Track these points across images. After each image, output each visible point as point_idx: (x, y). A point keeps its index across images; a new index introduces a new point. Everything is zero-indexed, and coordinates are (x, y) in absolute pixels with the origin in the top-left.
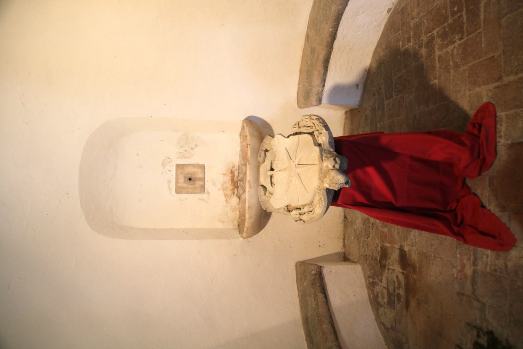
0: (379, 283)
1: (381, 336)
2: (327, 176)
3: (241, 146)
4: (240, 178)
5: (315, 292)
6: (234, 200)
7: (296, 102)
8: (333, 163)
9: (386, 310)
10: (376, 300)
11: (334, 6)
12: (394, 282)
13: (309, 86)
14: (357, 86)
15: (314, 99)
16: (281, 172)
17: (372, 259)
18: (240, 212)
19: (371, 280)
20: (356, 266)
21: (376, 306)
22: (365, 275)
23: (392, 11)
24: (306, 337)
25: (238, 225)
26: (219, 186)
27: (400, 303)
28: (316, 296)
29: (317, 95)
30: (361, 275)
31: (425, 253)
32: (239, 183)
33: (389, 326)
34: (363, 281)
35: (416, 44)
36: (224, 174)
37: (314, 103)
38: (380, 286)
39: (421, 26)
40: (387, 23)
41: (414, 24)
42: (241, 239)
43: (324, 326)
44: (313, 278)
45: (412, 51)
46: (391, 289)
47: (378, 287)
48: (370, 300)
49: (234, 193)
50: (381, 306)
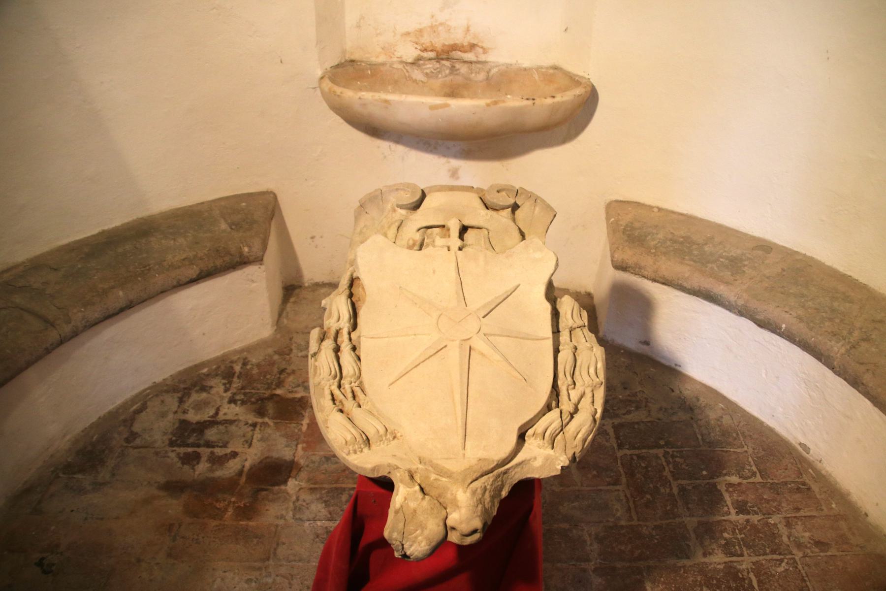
0: (229, 394)
1: (119, 402)
2: (426, 503)
3: (530, 69)
4: (457, 66)
5: (201, 259)
6: (409, 52)
7: (621, 199)
8: (466, 528)
9: (171, 416)
11: (843, 350)
12: (225, 446)
13: (656, 247)
14: (647, 343)
15: (628, 255)
16: (454, 274)
17: (282, 371)
18: (383, 64)
19: (237, 368)
20: (269, 327)
21: (182, 386)
22: (249, 349)
23: (804, 453)
24: (109, 231)
25: (353, 61)
26: (441, 17)
27: (179, 464)
28: (190, 261)
29: (636, 264)
31: (275, 554)
32: (447, 63)
33: (137, 428)
34: (237, 346)
35: (734, 532)
36: (468, 30)
37: (618, 256)
38: (222, 398)
39: (773, 552)
40: (777, 435)
41: (775, 525)
42: (319, 73)
43: (121, 293)
44: (233, 250)
46: (211, 434)
47: (222, 388)
48: (196, 366)
49: (425, 50)
50: (181, 401)
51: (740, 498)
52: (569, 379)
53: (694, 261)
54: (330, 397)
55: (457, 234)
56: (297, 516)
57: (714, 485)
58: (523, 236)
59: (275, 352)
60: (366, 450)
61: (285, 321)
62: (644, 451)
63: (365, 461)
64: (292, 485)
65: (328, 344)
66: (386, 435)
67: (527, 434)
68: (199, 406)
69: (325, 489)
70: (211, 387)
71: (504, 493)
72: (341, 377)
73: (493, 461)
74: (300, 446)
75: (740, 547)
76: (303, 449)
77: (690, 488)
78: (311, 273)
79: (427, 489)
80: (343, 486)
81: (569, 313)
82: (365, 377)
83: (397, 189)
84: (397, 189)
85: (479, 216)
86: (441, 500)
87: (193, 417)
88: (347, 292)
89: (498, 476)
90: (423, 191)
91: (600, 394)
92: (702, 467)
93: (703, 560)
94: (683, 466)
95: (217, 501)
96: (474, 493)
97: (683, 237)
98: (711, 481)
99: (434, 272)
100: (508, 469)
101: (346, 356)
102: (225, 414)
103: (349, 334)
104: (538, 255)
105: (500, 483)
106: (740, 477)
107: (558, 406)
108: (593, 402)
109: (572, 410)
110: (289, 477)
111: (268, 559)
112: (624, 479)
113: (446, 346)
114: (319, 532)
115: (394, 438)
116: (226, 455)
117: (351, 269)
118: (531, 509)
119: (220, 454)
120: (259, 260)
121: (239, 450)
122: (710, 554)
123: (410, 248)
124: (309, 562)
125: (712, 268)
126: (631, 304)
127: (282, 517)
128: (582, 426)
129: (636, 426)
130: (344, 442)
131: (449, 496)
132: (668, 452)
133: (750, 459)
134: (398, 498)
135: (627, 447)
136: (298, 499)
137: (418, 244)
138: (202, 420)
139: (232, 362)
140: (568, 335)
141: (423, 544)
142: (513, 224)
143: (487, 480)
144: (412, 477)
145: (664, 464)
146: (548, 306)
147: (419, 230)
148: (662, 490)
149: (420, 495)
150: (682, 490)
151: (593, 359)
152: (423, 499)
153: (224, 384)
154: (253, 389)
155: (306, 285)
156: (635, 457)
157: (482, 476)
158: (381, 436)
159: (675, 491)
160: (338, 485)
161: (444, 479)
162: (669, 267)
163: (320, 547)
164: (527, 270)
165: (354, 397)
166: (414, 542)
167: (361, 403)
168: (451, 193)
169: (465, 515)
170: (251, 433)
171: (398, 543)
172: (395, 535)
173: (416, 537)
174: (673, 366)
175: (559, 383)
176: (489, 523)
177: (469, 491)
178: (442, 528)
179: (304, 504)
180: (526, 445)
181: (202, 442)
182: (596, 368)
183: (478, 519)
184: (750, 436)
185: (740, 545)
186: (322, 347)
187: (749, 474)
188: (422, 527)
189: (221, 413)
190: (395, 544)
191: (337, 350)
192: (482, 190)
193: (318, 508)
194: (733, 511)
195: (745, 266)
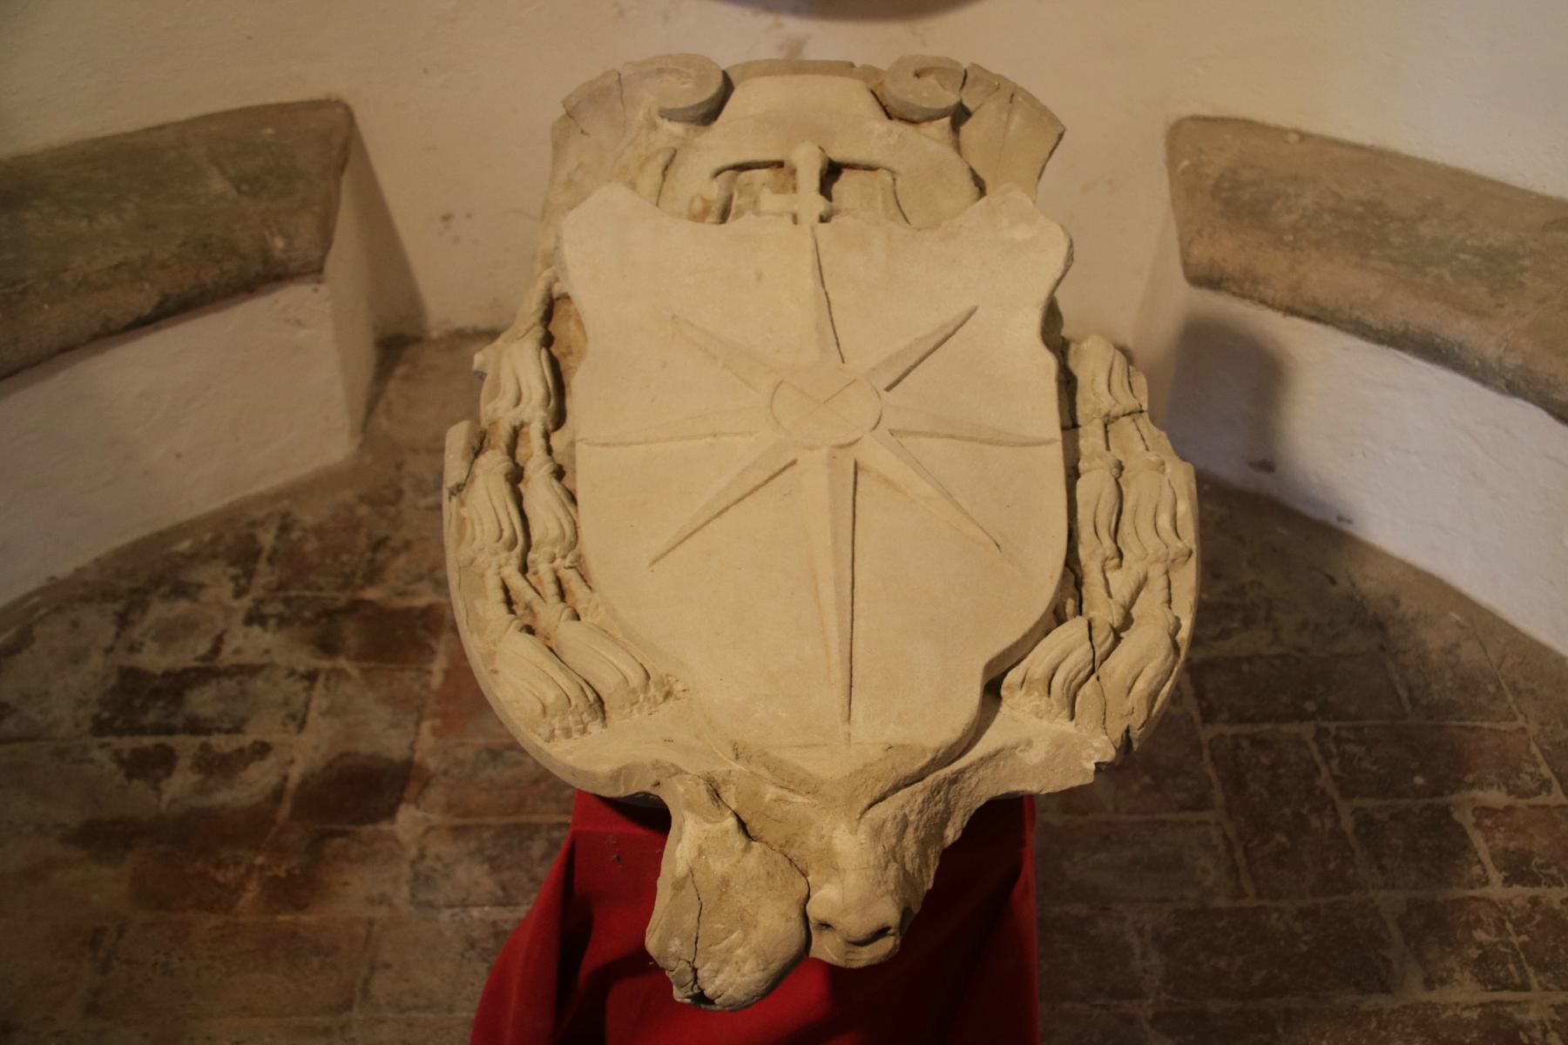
0: (247, 602)
2: (754, 860)
5: (163, 266)
7: (1206, 112)
8: (858, 925)
9: (96, 661)
10: (157, 581)
12: (237, 729)
14: (1267, 466)
15: (1226, 249)
16: (809, 282)
17: (379, 544)
19: (267, 539)
21: (125, 584)
22: (293, 492)
27: (120, 778)
30: (300, 467)
31: (366, 993)
35: (1501, 928)
38: (229, 612)
45: (1459, 893)
46: (203, 701)
47: (228, 589)
48: (161, 534)
50: (123, 621)
51: (1512, 845)
52: (1107, 542)
53: (1393, 261)
54: (500, 595)
55: (816, 184)
56: (422, 897)
57: (1446, 811)
58: (981, 188)
59: (362, 499)
60: (595, 728)
61: (384, 423)
62: (1267, 726)
63: (595, 757)
64: (408, 820)
65: (494, 462)
66: (646, 687)
67: (1006, 681)
68: (168, 634)
69: (488, 827)
70: (201, 586)
71: (952, 834)
72: (528, 546)
73: (924, 751)
74: (426, 726)
75: (1520, 968)
76: (434, 731)
77: (1384, 816)
78: (445, 301)
79: (755, 826)
80: (535, 819)
81: (1102, 379)
82: (590, 543)
83: (660, 71)
84: (660, 71)
85: (871, 137)
86: (793, 852)
87: (153, 659)
88: (538, 333)
89: (937, 789)
90: (725, 74)
91: (1187, 581)
92: (1414, 765)
93: (1425, 997)
94: (1366, 764)
95: (218, 866)
96: (877, 833)
97: (1362, 204)
98: (1437, 801)
99: (759, 277)
100: (962, 772)
101: (540, 492)
102: (237, 651)
103: (547, 436)
104: (1021, 234)
105: (941, 807)
106: (1510, 793)
107: (1079, 611)
108: (1169, 601)
109: (1116, 618)
110: (399, 801)
111: (348, 1005)
112: (1218, 797)
113: (794, 463)
114: (476, 934)
115: (668, 695)
116: (241, 751)
117: (547, 273)
118: (1015, 872)
119: (227, 750)
120: (313, 271)
121: (274, 737)
122: (1443, 981)
123: (699, 217)
124: (451, 1010)
125: (1439, 278)
126: (1216, 387)
127: (383, 900)
128: (1144, 662)
129: (1245, 668)
130: (539, 708)
131: (813, 841)
132: (1327, 731)
133: (1534, 749)
134: (684, 847)
135: (1225, 716)
136: (422, 856)
137: (716, 208)
138: (179, 666)
139: (253, 524)
140: (1101, 432)
141: (747, 968)
142: (954, 156)
143: (909, 800)
144: (716, 795)
145: (1318, 758)
146: (1049, 361)
147: (718, 173)
148: (1315, 822)
149: (738, 841)
150: (1365, 822)
151: (1167, 493)
152: (747, 849)
153: (235, 578)
154: (307, 587)
155: (435, 334)
156: (1245, 743)
157: (896, 789)
158: (634, 691)
159: (1348, 824)
160: (523, 819)
161: (798, 799)
162: (1328, 276)
163: (477, 977)
164: (987, 277)
165: (562, 594)
166: (725, 961)
167: (580, 609)
168: (797, 79)
169: (854, 890)
170: (303, 696)
171: (683, 965)
172: (675, 946)
173: (729, 950)
174: (1333, 521)
175: (1083, 553)
176: (916, 910)
177: (863, 827)
178: (795, 924)
179: (439, 866)
180: (1004, 709)
181: (178, 721)
182: (1174, 517)
183: (888, 899)
184: (1533, 692)
185: (1517, 960)
186: (478, 470)
187: (1533, 786)
188: (745, 922)
189: (227, 650)
190: (676, 968)
191: (516, 477)
192: (876, 72)
193: (474, 876)
194: (1496, 877)
195: (1524, 270)
